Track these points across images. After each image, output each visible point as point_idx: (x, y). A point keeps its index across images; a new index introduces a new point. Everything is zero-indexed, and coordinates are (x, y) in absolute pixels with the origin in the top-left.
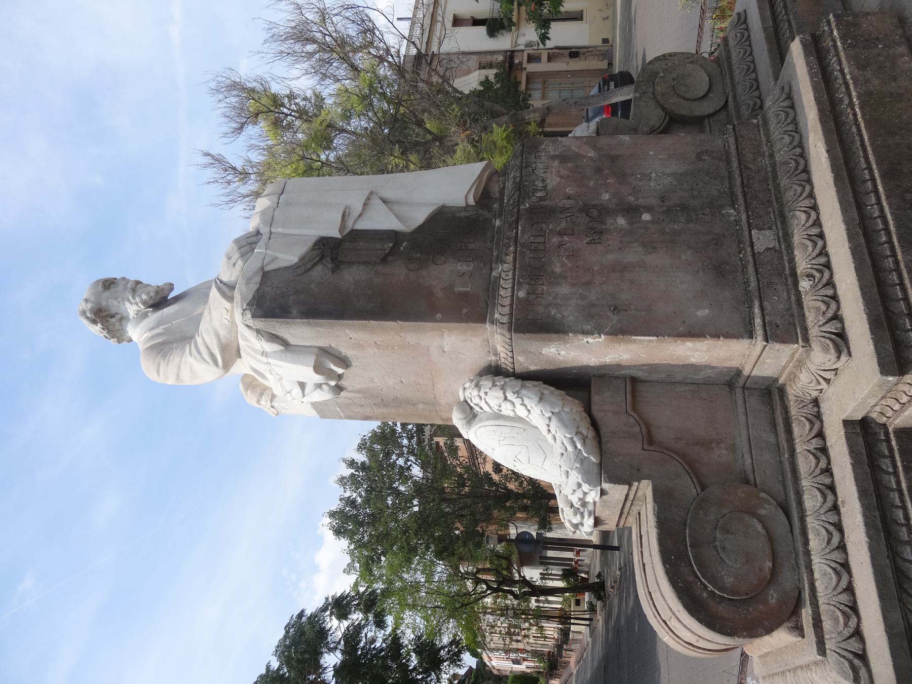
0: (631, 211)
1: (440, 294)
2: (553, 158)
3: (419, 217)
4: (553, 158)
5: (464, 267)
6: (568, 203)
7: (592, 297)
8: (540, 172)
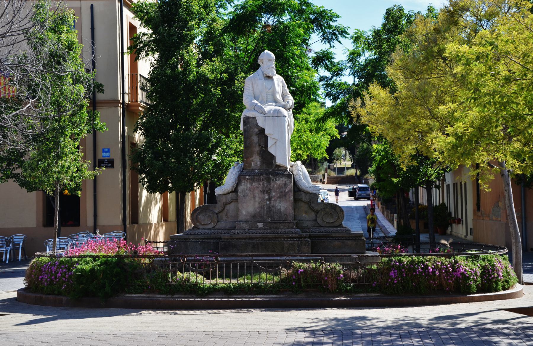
0: (270, 199)
1: (251, 159)
2: (285, 182)
4: (285, 182)
5: (258, 164)
6: (272, 186)
7: (247, 191)
8: (281, 179)
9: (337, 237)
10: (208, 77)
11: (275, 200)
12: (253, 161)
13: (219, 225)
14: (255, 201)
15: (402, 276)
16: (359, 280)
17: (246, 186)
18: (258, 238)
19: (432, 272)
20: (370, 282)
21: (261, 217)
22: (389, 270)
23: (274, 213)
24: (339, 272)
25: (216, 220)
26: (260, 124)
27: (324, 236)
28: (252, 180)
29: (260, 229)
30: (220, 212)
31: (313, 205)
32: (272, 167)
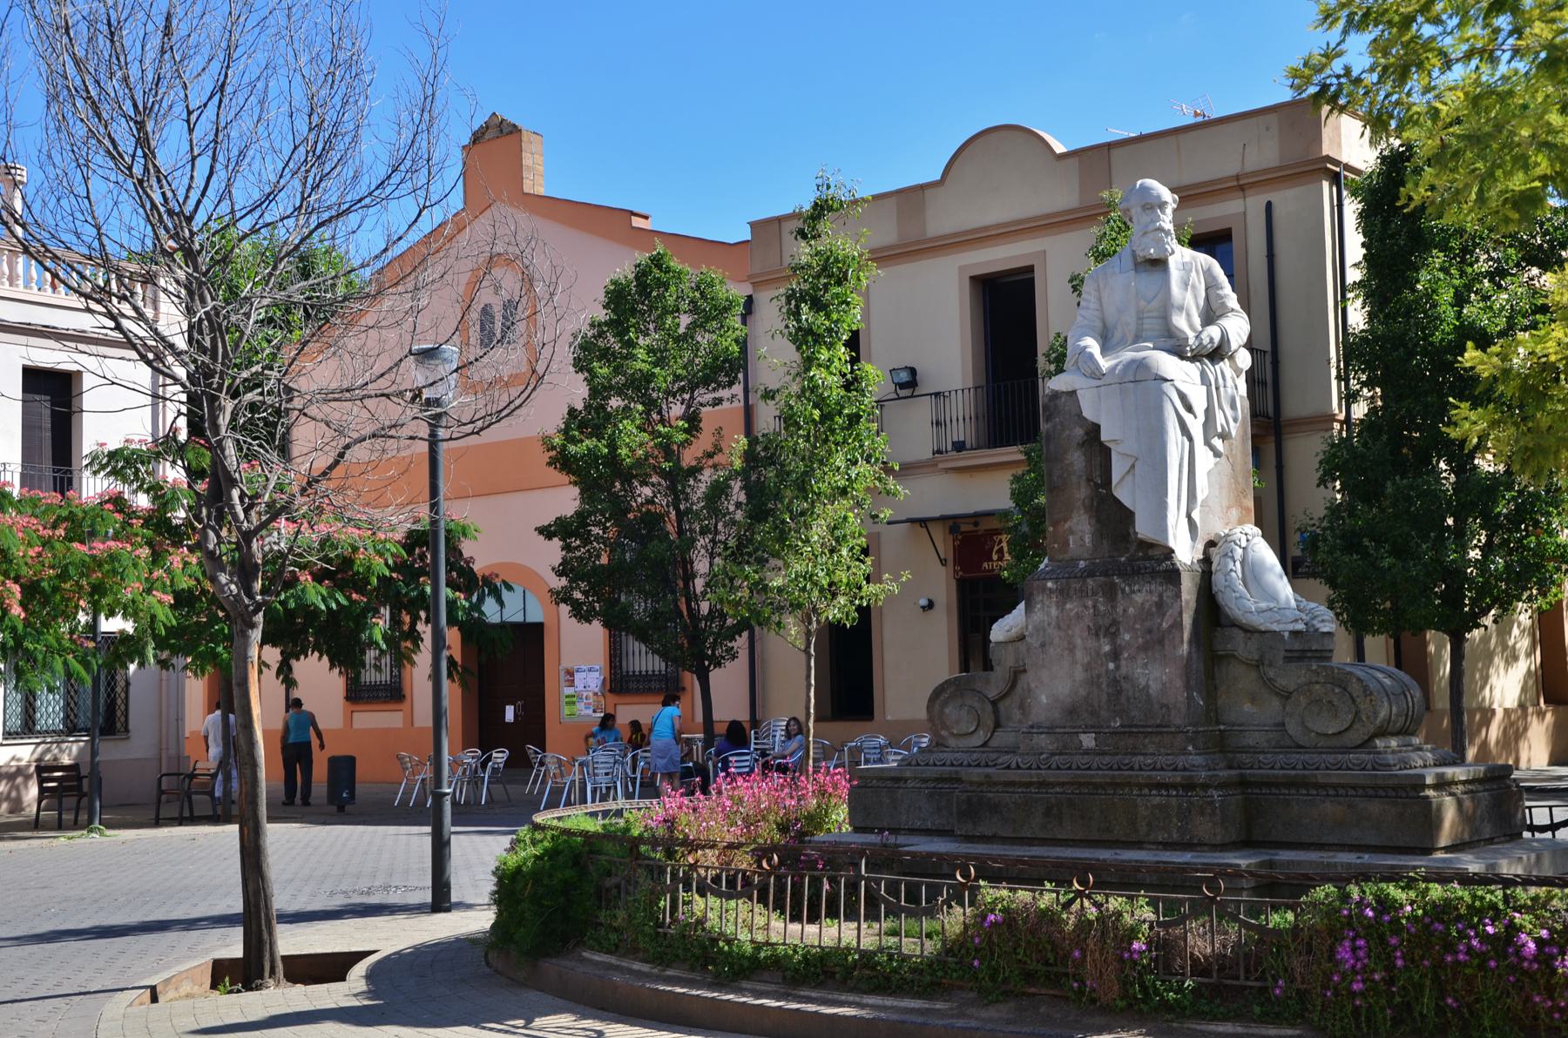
0: (1115, 655)
2: (1161, 596)
3: (1126, 499)
4: (1161, 596)
6: (1120, 610)
7: (1050, 631)
9: (1335, 787)
10: (1484, 329)
11: (1132, 658)
12: (1072, 532)
13: (1002, 738)
14: (1074, 662)
15: (1389, 968)
16: (1221, 969)
17: (1048, 614)
18: (1062, 784)
19: (1536, 959)
20: (1262, 978)
21: (1093, 713)
22: (1334, 934)
23: (1128, 699)
24: (1132, 933)
25: (990, 723)
26: (1088, 413)
27: (1292, 784)
28: (1064, 594)
29: (1087, 752)
30: (1003, 697)
31: (1271, 674)
32: (1127, 550)
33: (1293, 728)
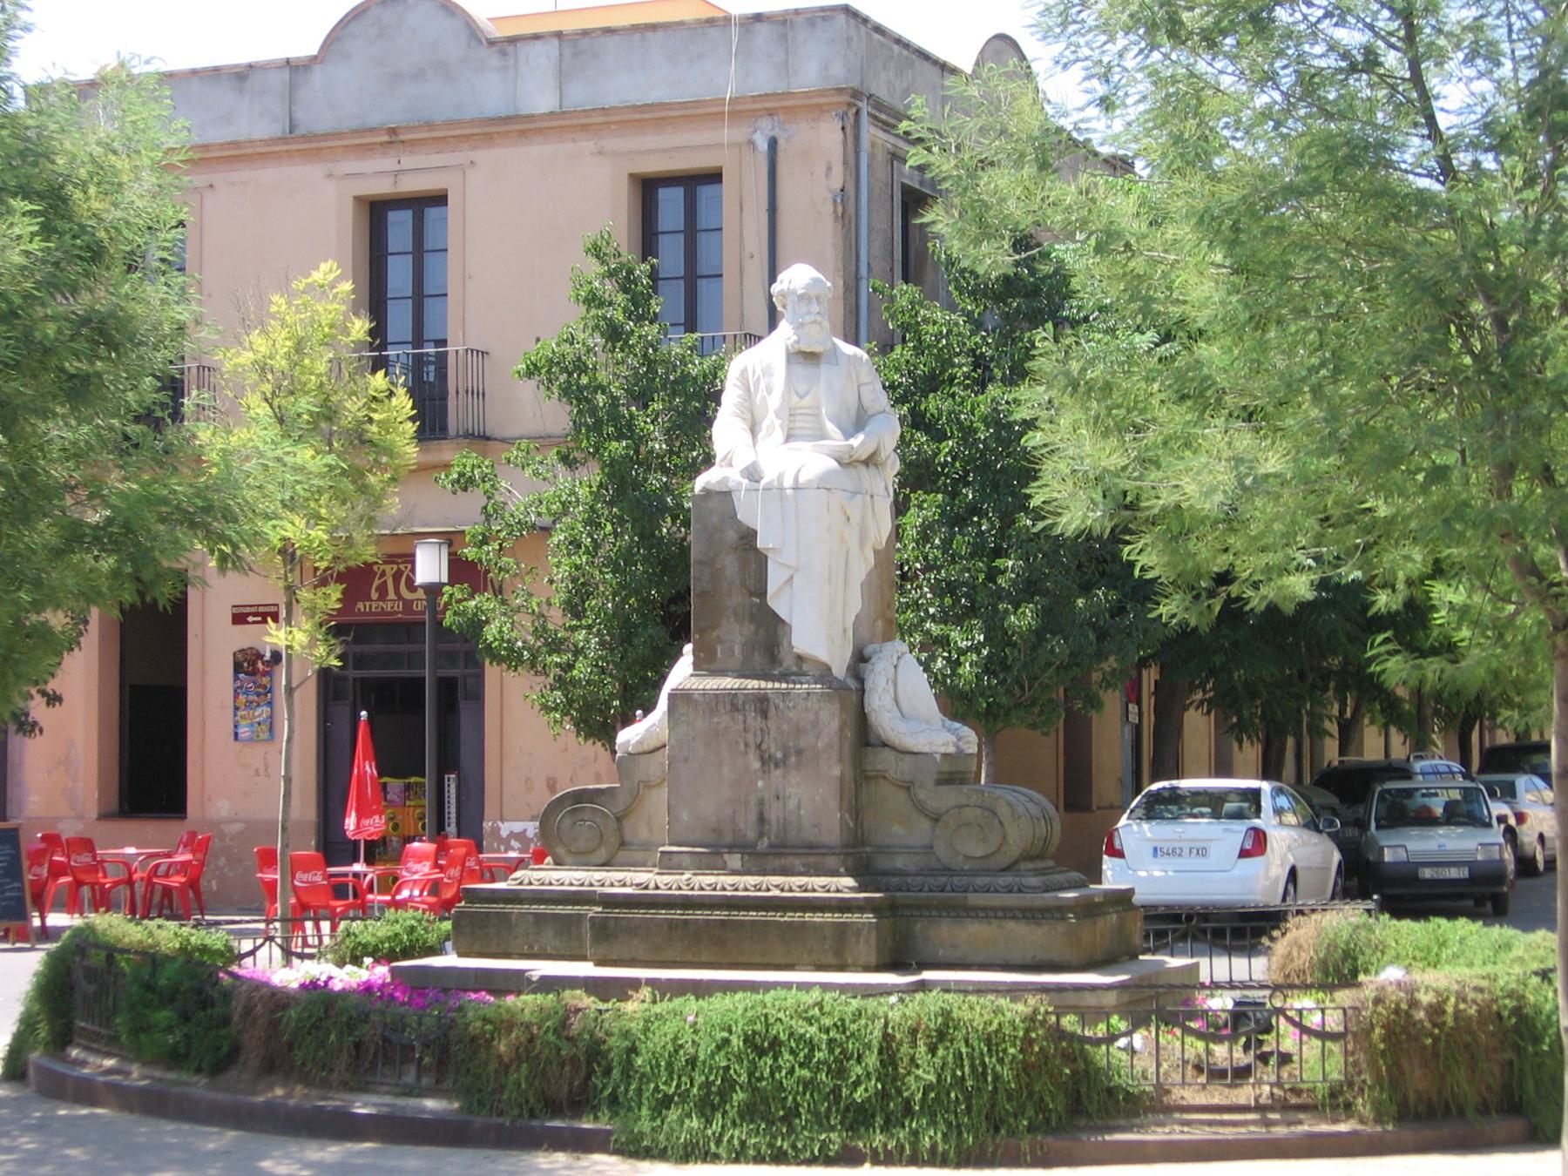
1: (714, 634)
33: (941, 850)
